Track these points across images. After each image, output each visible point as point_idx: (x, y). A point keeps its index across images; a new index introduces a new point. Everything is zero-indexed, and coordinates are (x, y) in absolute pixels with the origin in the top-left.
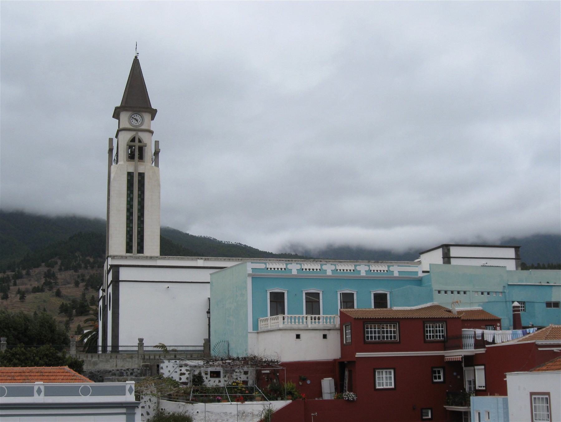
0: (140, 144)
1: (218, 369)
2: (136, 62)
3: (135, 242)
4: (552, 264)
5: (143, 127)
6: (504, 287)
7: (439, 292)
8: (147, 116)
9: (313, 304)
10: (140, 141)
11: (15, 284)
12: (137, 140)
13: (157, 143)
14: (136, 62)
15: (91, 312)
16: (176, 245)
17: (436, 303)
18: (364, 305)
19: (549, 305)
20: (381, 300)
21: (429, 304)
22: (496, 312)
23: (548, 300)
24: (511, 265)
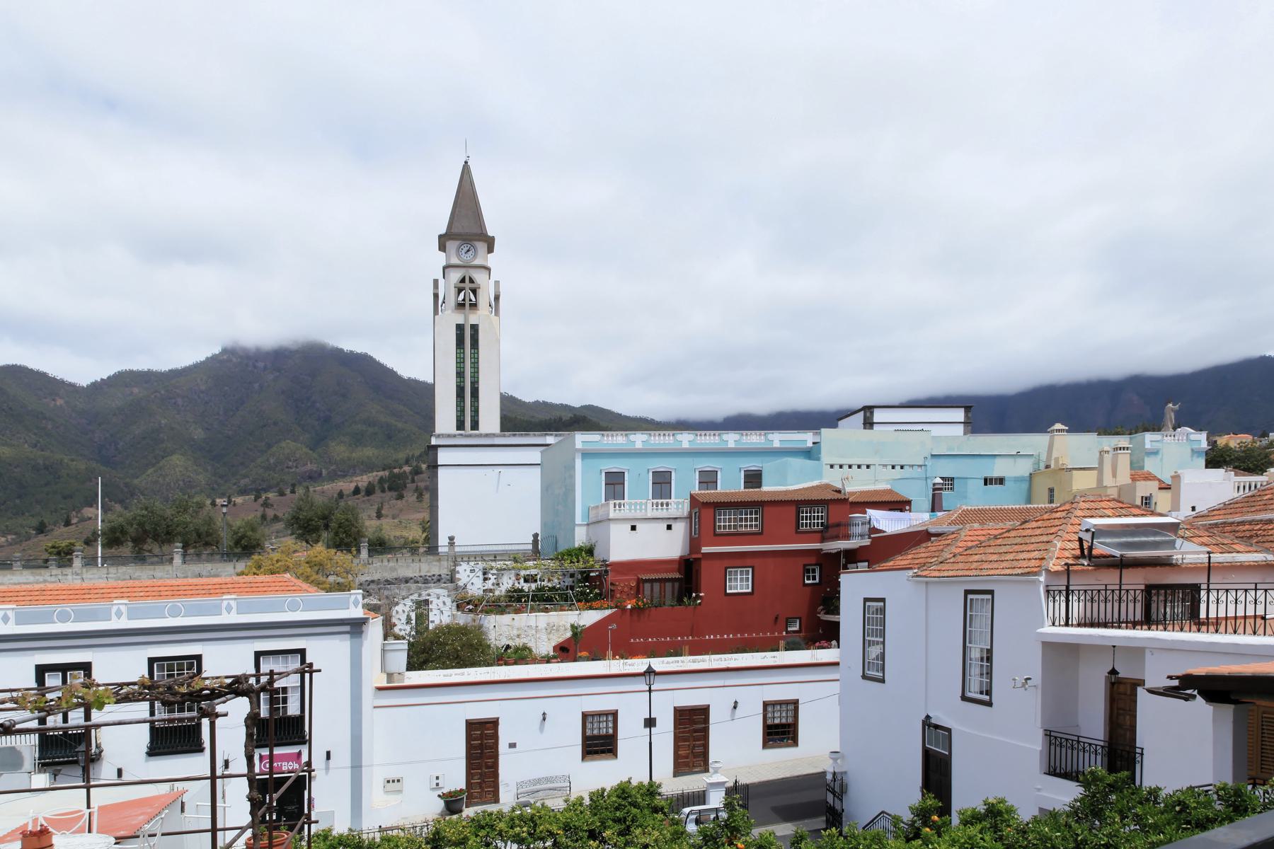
0: (472, 286)
1: (533, 572)
2: (466, 169)
3: (467, 418)
4: (561, 419)
5: (476, 262)
6: (926, 458)
7: (832, 466)
8: (482, 247)
9: (662, 483)
10: (471, 281)
11: (413, 481)
12: (467, 280)
13: (497, 283)
14: (466, 169)
15: (858, 530)
16: (523, 419)
17: (825, 481)
18: (731, 484)
19: (987, 481)
20: (754, 479)
21: (815, 483)
22: (905, 492)
23: (989, 475)
24: (960, 429)
